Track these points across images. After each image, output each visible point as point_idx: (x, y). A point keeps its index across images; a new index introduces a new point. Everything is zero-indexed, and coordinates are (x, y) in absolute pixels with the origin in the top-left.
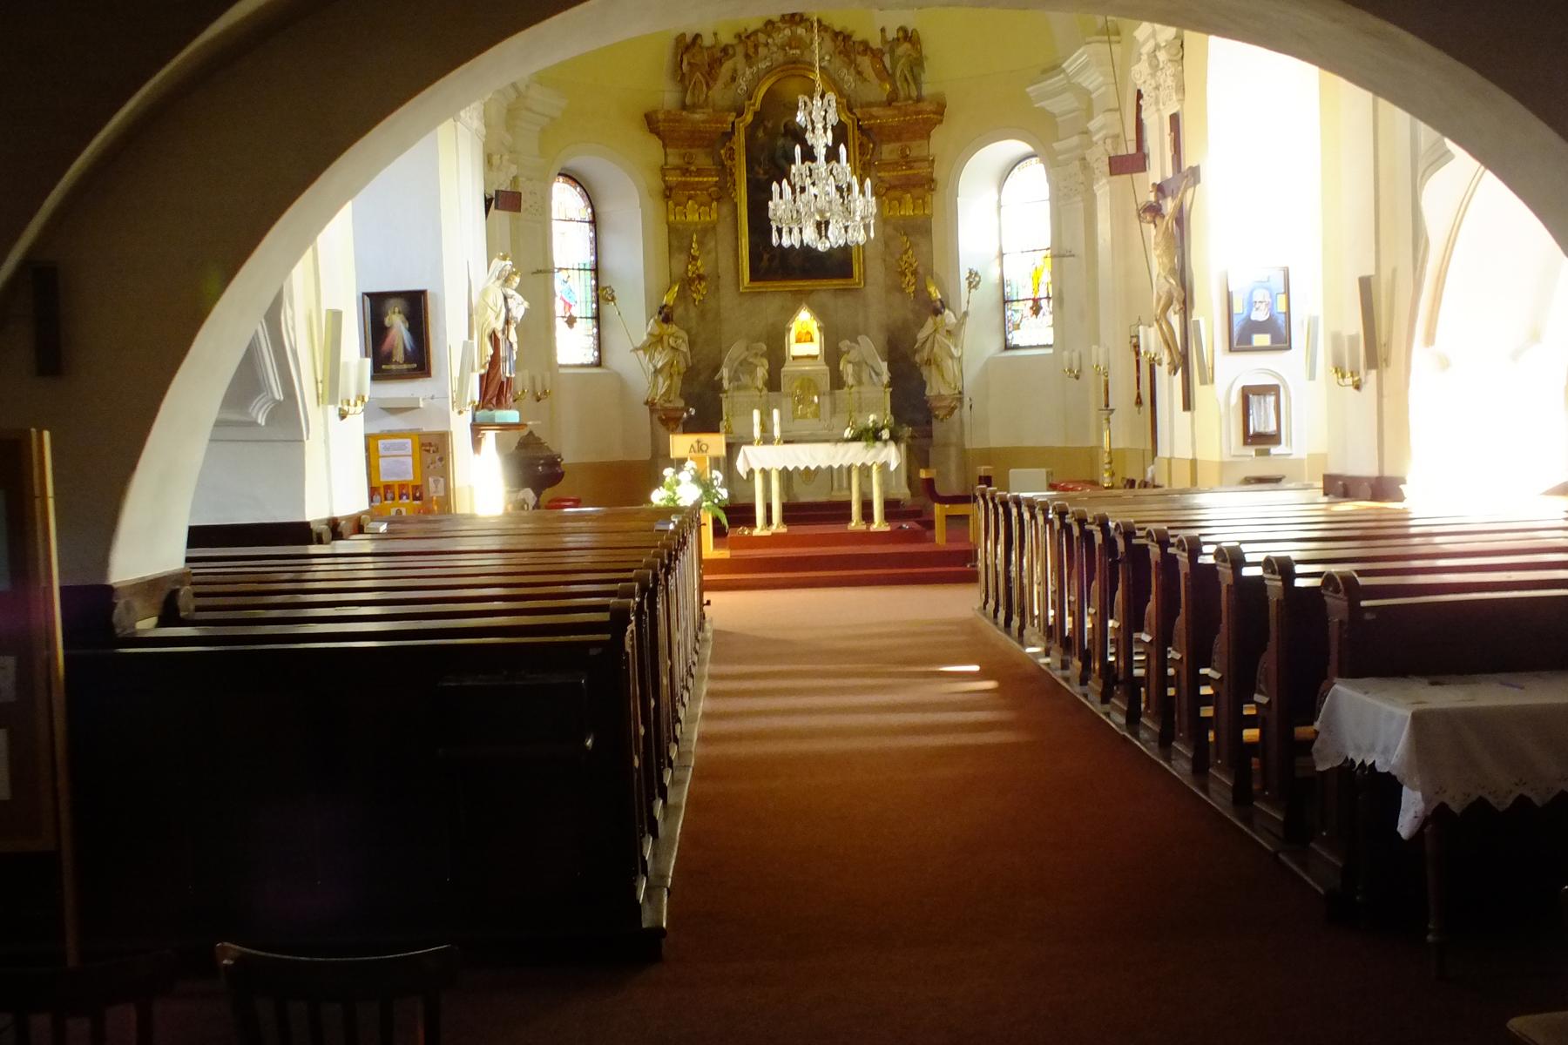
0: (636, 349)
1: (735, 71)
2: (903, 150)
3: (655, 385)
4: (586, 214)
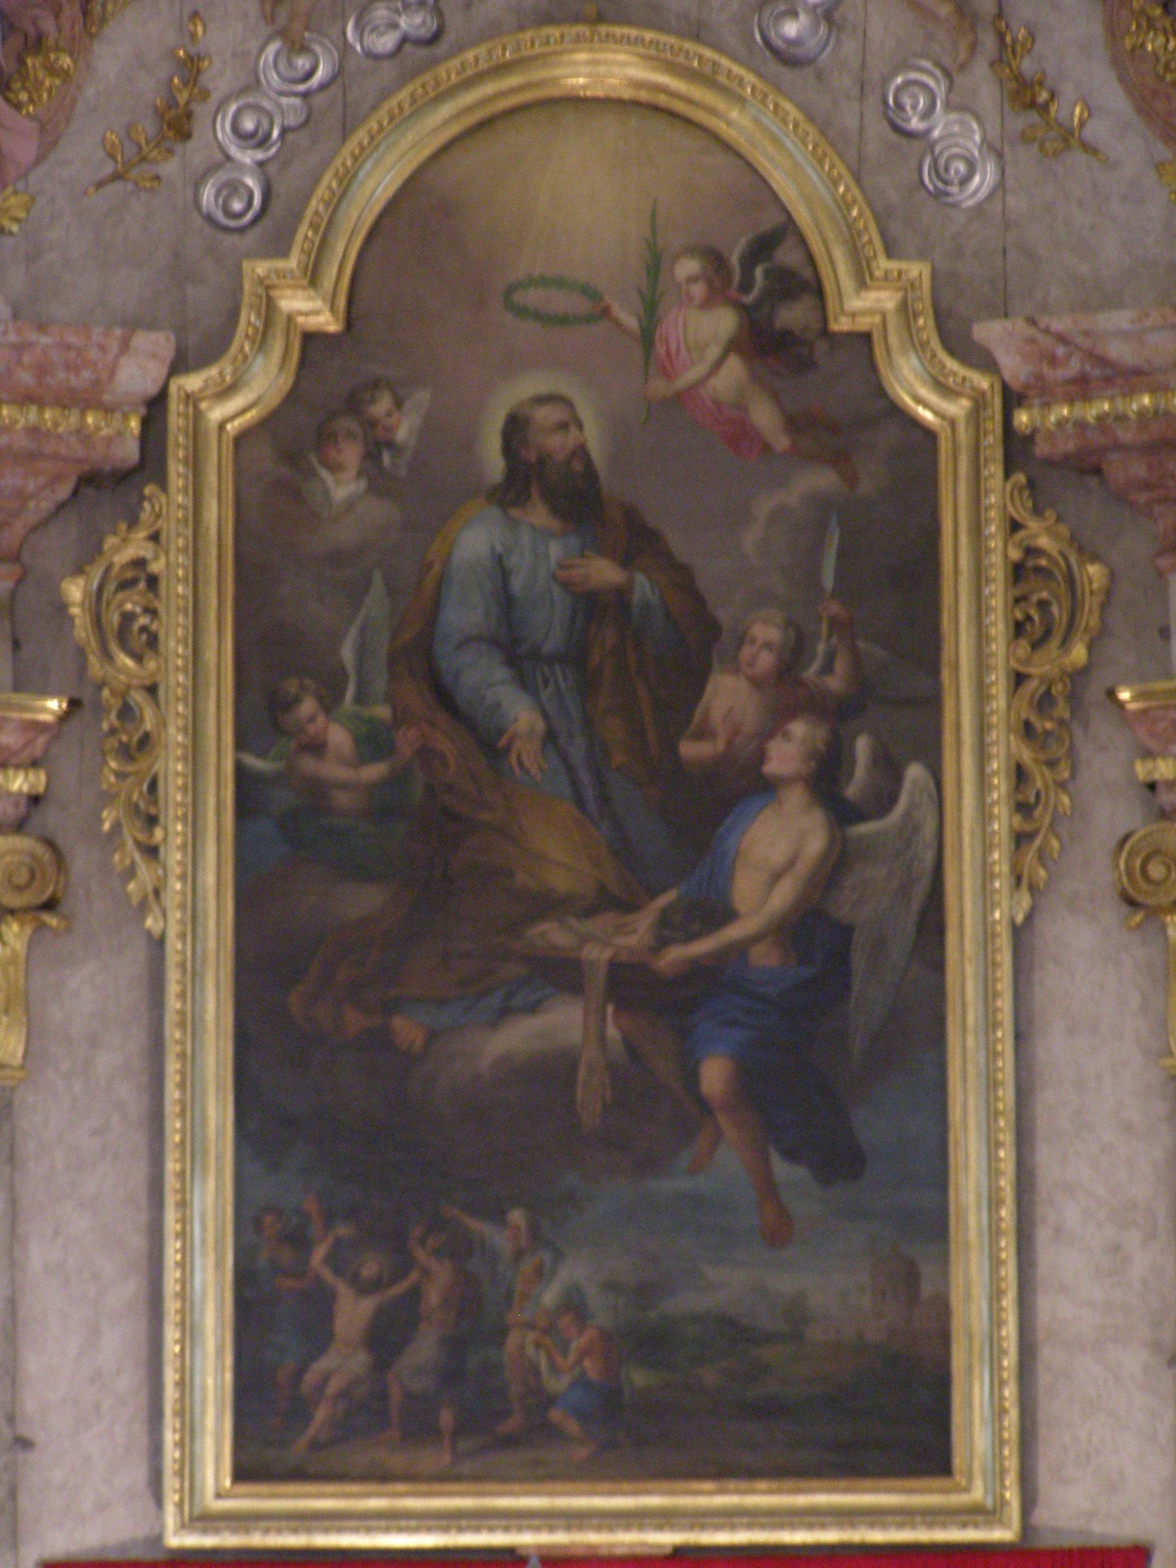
1: (191, 68)
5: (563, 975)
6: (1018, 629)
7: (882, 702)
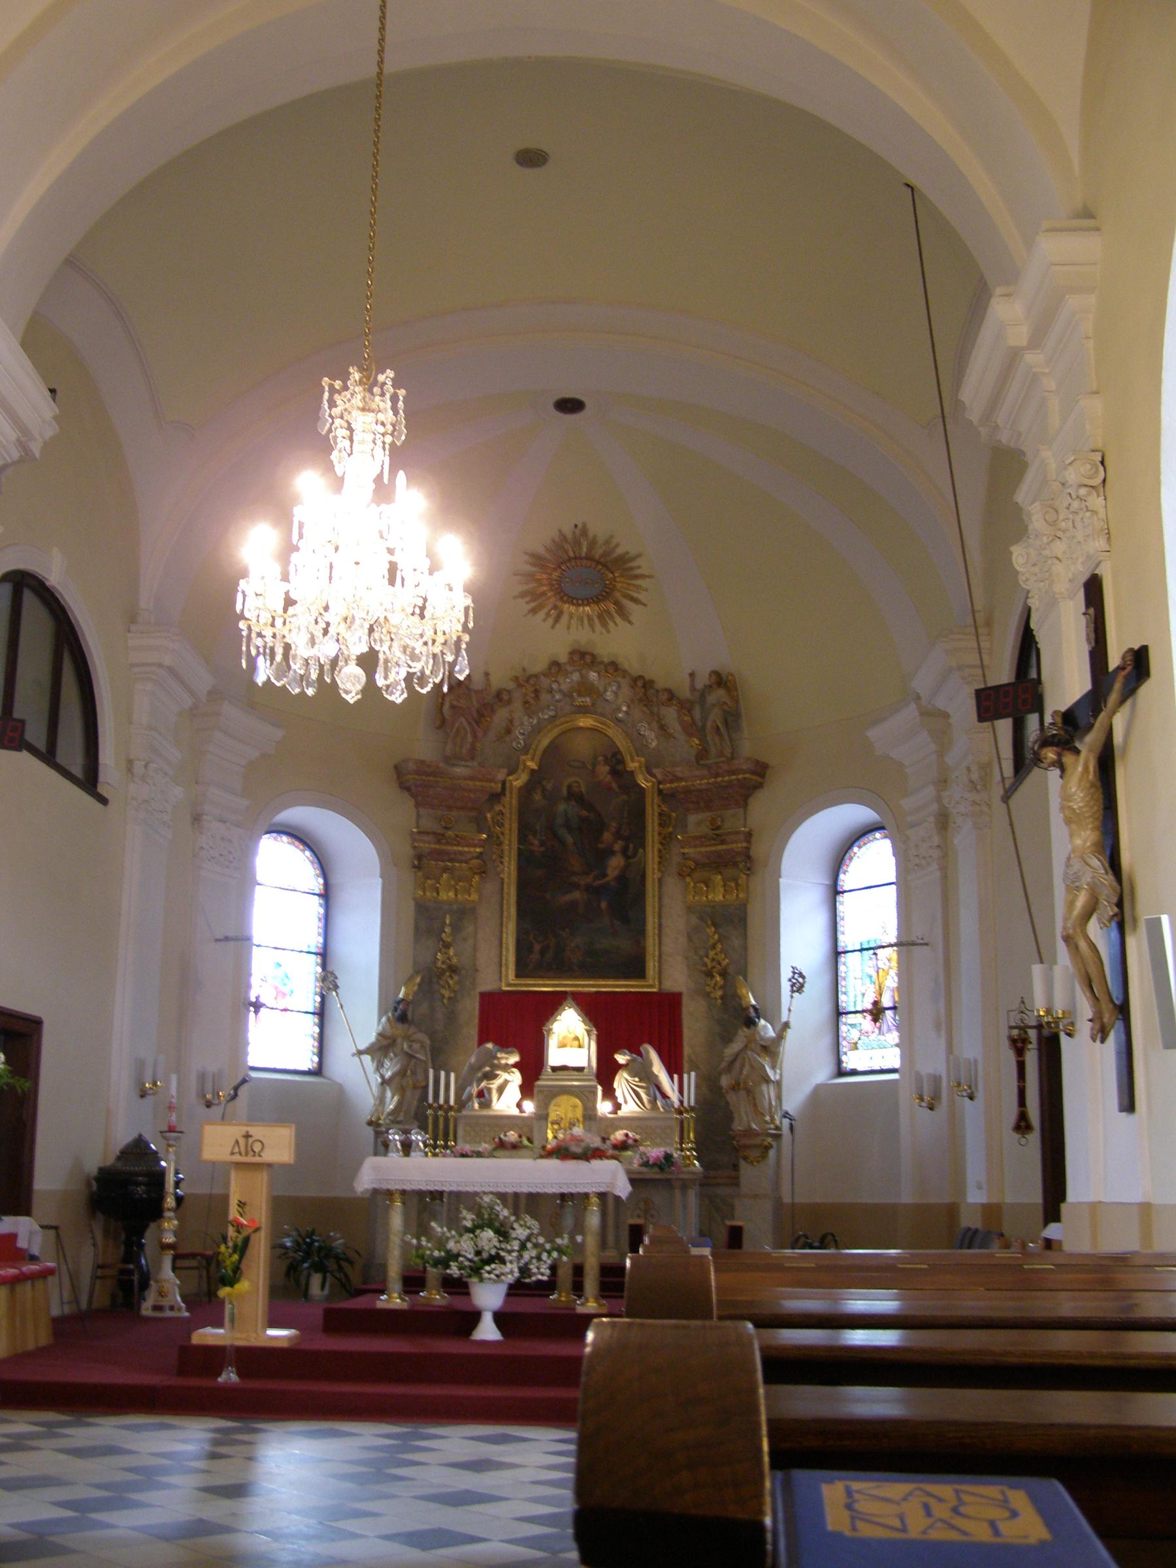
0: (360, 1053)
1: (511, 721)
2: (713, 821)
3: (381, 1100)
4: (317, 884)
5: (576, 886)
6: (660, 825)
7: (635, 837)
